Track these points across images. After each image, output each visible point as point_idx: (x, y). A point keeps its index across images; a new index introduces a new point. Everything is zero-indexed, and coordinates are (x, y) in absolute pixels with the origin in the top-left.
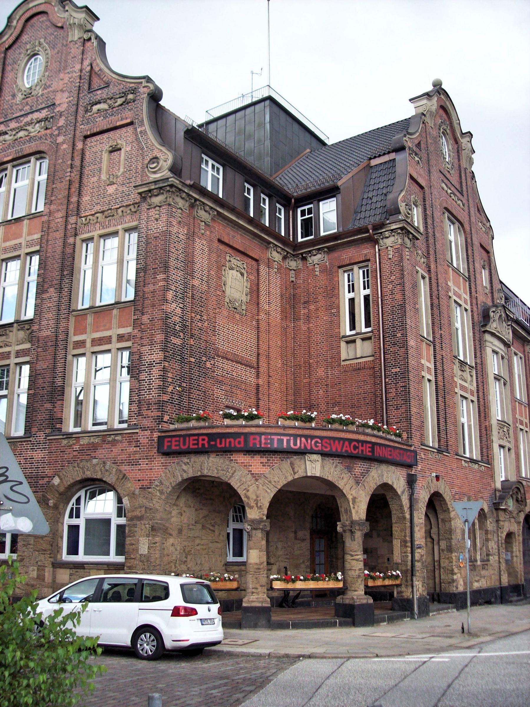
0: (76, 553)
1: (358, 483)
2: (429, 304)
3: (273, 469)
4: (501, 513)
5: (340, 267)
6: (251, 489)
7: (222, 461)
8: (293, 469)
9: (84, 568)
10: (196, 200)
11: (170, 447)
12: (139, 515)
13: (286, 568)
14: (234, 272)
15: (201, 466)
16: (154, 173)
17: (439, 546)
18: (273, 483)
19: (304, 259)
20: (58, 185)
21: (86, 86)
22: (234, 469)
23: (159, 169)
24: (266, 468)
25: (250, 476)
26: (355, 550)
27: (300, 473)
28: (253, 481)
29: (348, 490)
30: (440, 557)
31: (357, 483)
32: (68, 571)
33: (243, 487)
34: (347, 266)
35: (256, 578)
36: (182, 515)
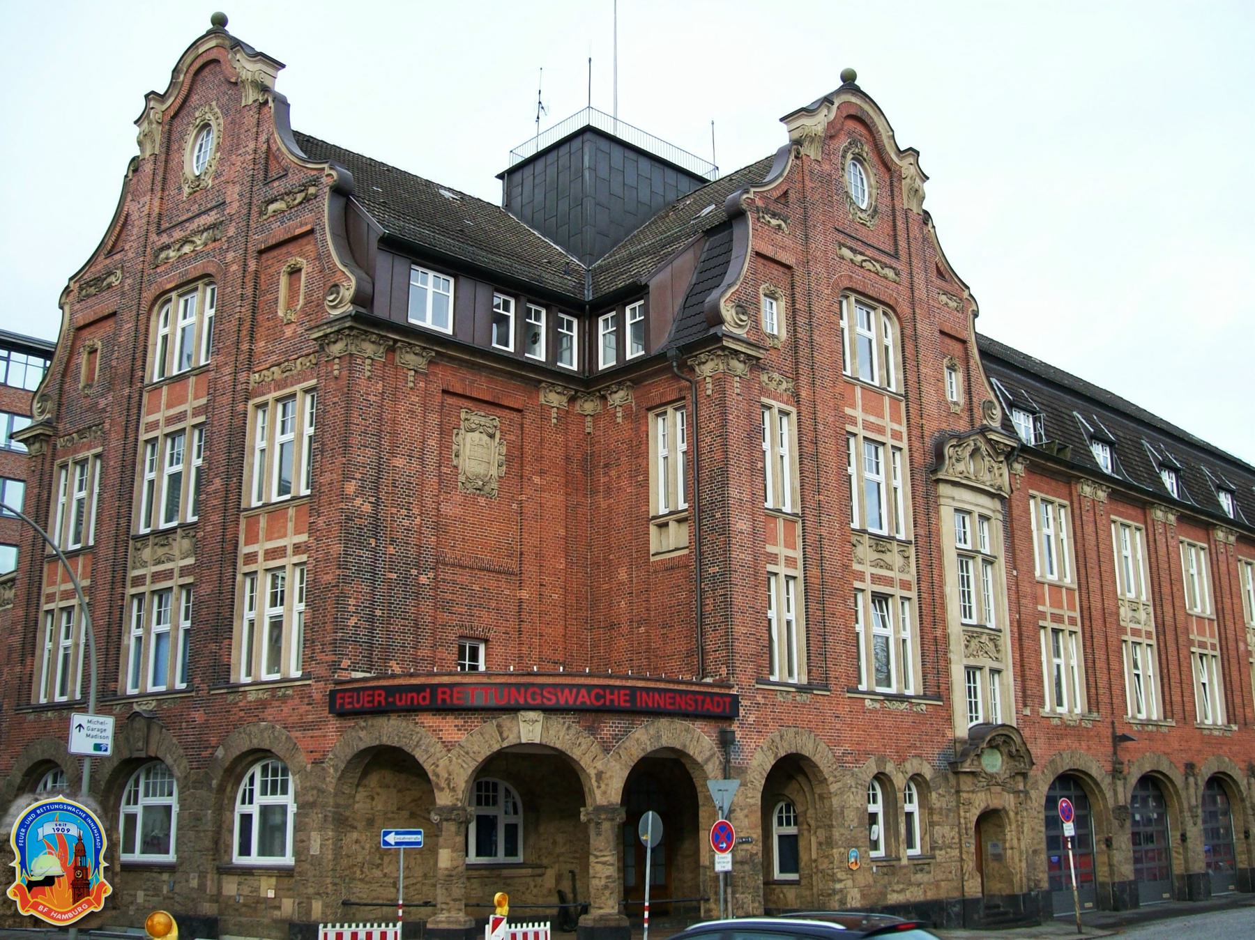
0: (248, 854)
1: (606, 750)
2: (796, 454)
4: (966, 783)
5: (649, 409)
6: (441, 763)
7: (404, 724)
8: (501, 734)
9: (253, 875)
10: (396, 341)
11: (348, 704)
12: (311, 799)
13: (571, 872)
14: (476, 435)
16: (334, 307)
19: (604, 398)
20: (225, 326)
21: (261, 176)
23: (340, 302)
27: (512, 740)
28: (444, 752)
29: (589, 761)
32: (236, 879)
33: (431, 761)
34: (659, 408)
36: (373, 799)
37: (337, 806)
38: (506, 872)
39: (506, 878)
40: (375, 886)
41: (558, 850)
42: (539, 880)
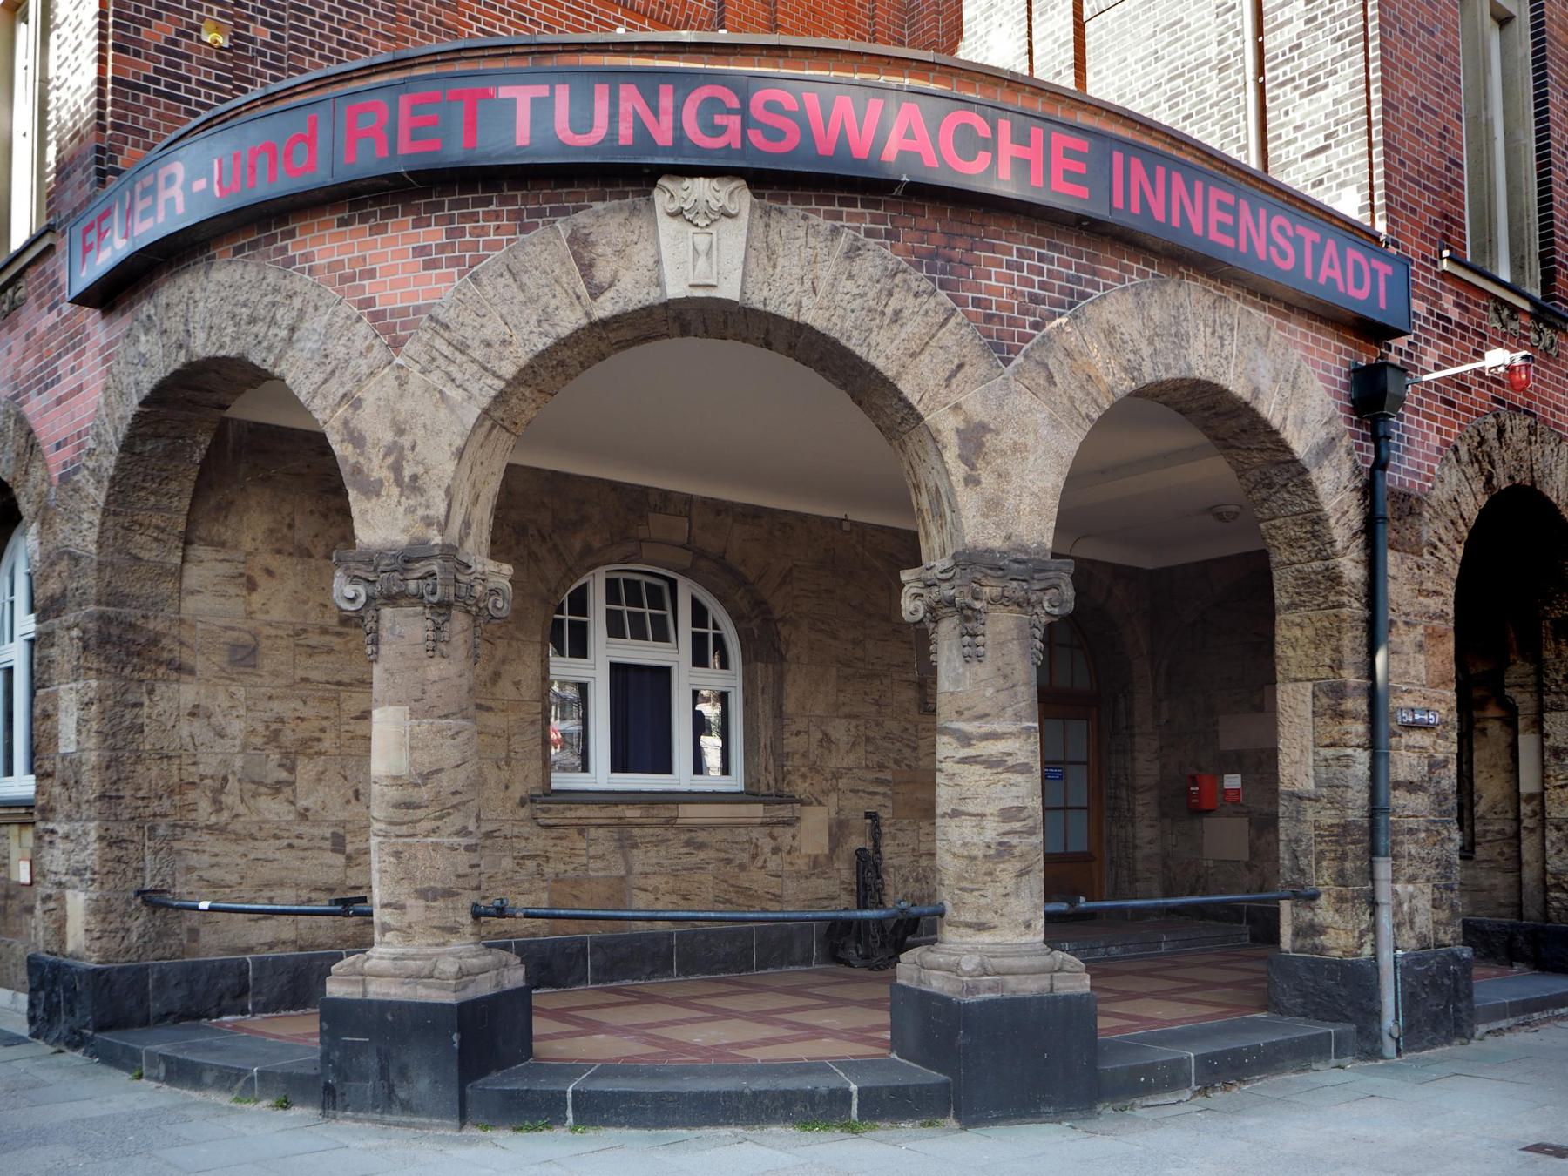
1: (1001, 349)
3: (475, 279)
6: (370, 395)
7: (251, 273)
8: (587, 268)
15: (186, 322)
17: (1543, 736)
18: (478, 354)
22: (297, 302)
24: (439, 279)
25: (364, 328)
26: (982, 708)
28: (378, 353)
30: (1544, 778)
31: (998, 348)
35: (397, 854)
36: (252, 586)
37: (113, 597)
38: (689, 813)
39: (693, 828)
40: (266, 848)
41: (834, 762)
42: (785, 834)
